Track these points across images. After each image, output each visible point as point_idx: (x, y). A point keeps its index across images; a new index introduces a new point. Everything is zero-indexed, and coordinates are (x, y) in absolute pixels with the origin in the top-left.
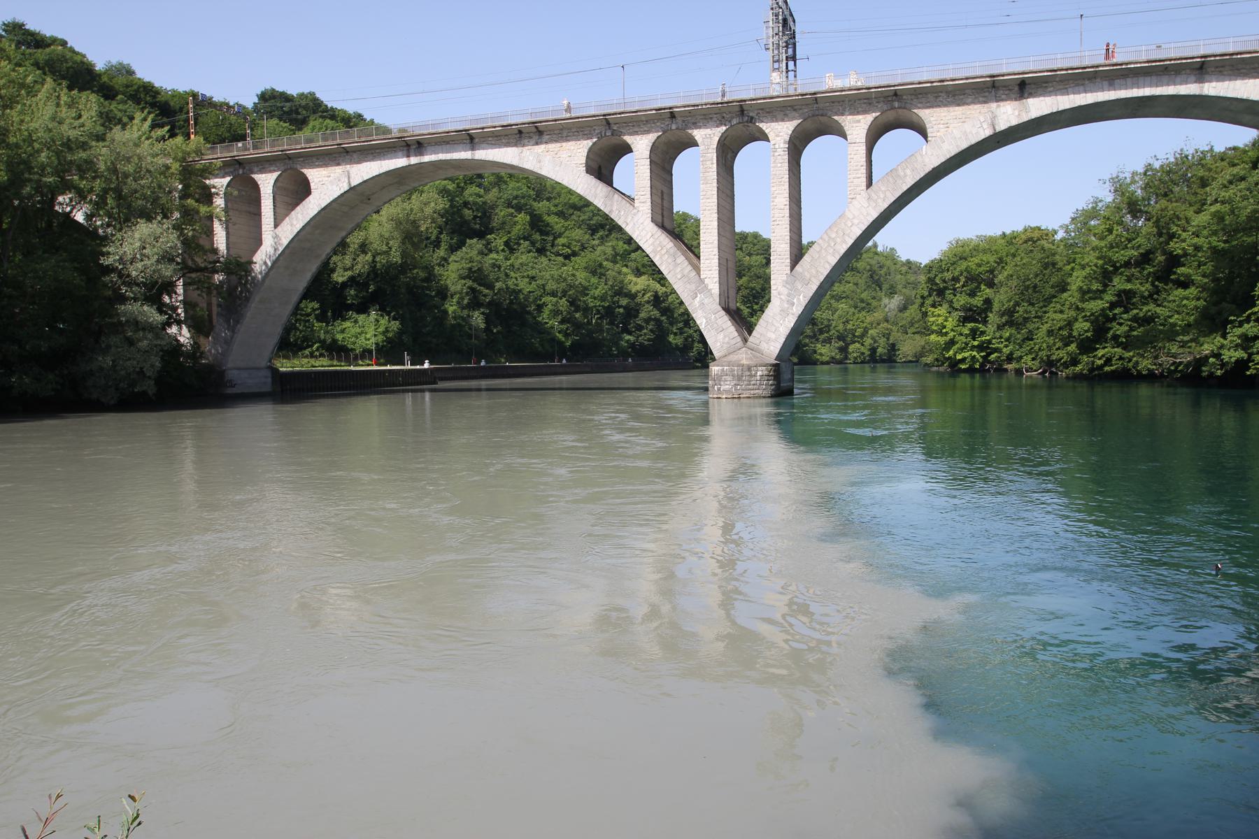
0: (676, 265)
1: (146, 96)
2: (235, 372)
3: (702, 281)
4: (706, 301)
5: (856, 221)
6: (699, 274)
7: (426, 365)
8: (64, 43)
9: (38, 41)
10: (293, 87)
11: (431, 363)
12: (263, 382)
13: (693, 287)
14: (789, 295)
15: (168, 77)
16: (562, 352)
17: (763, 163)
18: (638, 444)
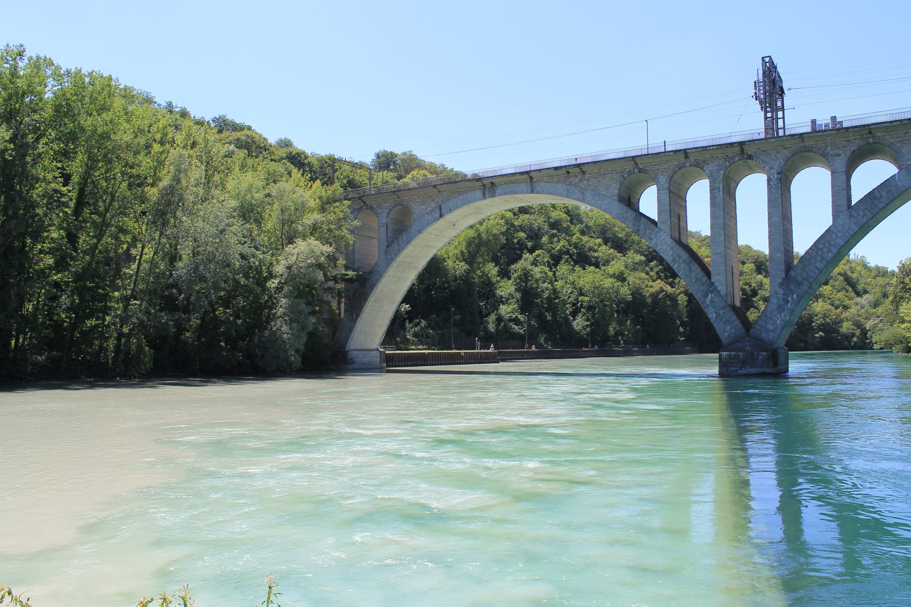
0: (691, 271)
1: (297, 160)
2: (356, 352)
3: (713, 284)
4: (716, 299)
5: (840, 235)
6: (710, 278)
7: (491, 350)
8: (249, 128)
9: (237, 128)
10: (398, 148)
11: (495, 348)
12: (375, 358)
13: (705, 288)
14: (784, 294)
15: (314, 145)
16: (520, 340)
17: (752, 192)
18: (339, 303)
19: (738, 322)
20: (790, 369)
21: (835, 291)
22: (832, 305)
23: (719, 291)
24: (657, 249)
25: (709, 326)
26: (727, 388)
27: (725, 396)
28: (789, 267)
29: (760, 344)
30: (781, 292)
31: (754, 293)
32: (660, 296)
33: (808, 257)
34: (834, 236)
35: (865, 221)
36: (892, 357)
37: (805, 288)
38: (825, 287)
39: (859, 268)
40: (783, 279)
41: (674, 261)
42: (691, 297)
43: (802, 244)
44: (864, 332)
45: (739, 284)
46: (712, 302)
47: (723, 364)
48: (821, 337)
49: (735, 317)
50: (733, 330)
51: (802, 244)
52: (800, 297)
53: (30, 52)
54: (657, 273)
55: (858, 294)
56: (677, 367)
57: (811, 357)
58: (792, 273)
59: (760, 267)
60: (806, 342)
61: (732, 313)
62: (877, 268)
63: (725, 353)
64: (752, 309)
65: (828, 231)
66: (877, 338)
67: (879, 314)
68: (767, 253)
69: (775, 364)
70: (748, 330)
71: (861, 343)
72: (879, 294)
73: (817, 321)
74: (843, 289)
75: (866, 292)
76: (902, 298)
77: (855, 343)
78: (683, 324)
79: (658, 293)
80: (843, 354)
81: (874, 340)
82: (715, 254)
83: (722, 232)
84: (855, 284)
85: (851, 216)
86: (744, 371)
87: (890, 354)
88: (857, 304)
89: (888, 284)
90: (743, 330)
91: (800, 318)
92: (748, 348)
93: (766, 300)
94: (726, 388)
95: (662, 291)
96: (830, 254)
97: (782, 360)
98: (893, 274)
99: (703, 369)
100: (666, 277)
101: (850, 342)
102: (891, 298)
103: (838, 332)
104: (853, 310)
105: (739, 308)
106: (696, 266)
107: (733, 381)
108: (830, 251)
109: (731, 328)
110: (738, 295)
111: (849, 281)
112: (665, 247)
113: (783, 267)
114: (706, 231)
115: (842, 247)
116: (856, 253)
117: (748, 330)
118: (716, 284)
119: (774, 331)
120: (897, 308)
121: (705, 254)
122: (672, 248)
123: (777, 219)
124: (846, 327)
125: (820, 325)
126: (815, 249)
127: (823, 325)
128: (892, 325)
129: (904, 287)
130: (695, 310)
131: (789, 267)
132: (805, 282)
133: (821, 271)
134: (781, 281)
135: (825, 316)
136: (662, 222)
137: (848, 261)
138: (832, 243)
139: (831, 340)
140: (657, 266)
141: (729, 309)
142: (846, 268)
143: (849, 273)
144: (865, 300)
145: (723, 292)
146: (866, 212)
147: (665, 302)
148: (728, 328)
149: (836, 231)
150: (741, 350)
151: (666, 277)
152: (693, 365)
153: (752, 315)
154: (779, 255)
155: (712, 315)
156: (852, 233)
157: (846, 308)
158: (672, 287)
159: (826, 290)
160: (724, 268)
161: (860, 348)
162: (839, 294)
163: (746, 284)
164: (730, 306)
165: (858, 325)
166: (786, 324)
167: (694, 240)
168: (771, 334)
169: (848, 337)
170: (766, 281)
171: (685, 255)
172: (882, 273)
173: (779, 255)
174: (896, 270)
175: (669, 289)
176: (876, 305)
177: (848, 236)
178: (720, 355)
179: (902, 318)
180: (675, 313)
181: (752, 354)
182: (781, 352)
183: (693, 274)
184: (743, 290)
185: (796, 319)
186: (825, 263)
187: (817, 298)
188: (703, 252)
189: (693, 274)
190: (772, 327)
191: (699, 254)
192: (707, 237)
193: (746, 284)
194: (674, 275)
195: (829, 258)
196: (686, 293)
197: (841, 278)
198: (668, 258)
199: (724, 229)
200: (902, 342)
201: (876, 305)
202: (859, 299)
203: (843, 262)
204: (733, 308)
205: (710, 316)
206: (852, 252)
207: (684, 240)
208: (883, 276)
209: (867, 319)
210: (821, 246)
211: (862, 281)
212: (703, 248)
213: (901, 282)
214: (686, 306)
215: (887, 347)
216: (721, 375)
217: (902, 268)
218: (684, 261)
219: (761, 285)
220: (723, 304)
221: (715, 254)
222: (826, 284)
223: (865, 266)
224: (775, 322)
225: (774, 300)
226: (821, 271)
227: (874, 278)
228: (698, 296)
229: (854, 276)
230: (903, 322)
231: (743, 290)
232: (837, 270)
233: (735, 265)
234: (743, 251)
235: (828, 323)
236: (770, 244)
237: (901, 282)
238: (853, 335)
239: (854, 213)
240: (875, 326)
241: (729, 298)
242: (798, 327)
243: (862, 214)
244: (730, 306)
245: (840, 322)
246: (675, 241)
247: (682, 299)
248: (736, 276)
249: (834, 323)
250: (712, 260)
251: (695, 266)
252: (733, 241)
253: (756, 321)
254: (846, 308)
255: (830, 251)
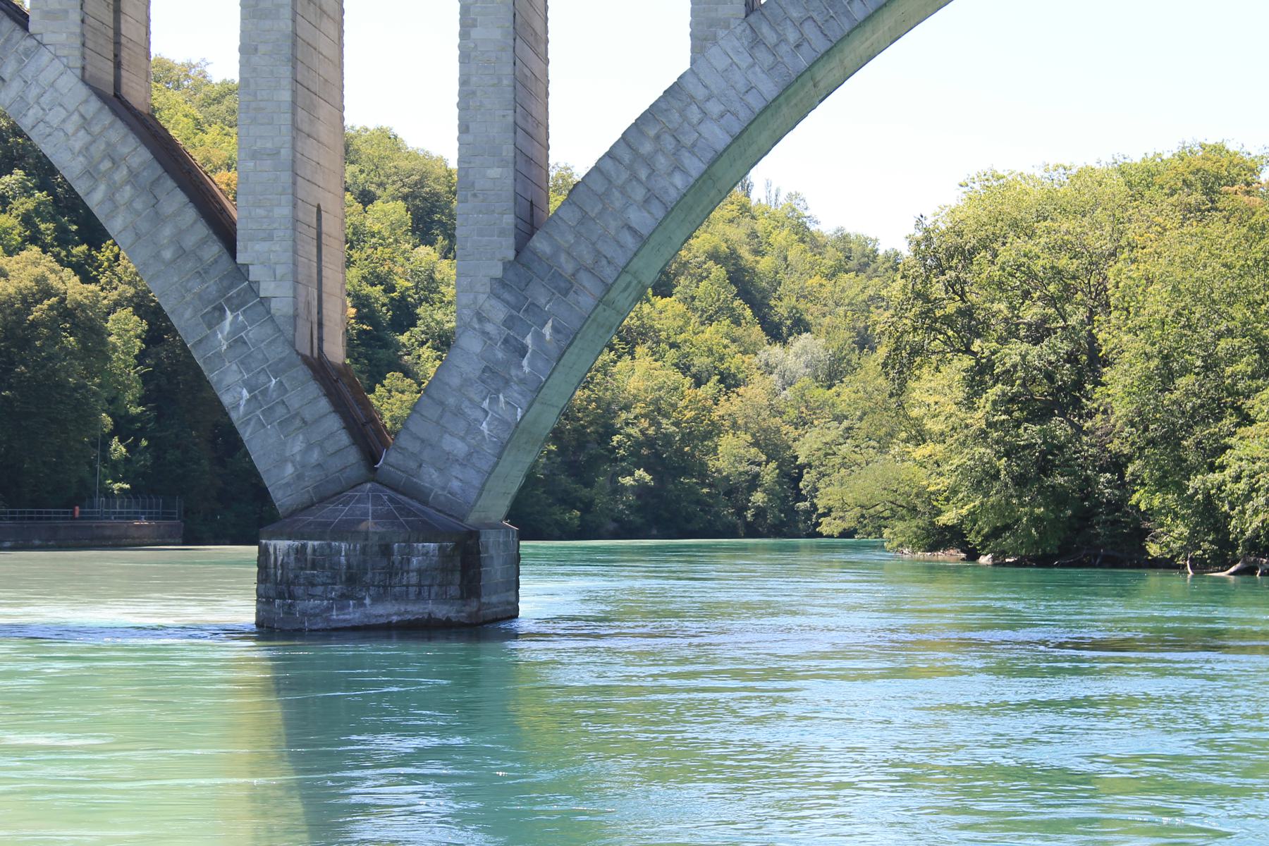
0: (158, 218)
3: (241, 272)
4: (252, 333)
5: (714, 108)
6: (232, 252)
13: (211, 286)
14: (509, 322)
19: (333, 423)
20: (522, 607)
21: (695, 319)
22: (684, 369)
23: (264, 301)
24: (26, 124)
25: (227, 440)
26: (284, 684)
27: (277, 712)
28: (530, 220)
29: (414, 510)
30: (499, 313)
31: (404, 315)
32: (37, 313)
33: (599, 186)
34: (694, 114)
35: (803, 63)
36: (878, 566)
37: (586, 301)
38: (660, 302)
39: (780, 237)
40: (507, 266)
41: (91, 173)
42: (158, 327)
43: (577, 141)
44: (792, 474)
45: (342, 282)
46: (237, 341)
47: (275, 589)
48: (641, 489)
49: (324, 404)
50: (315, 456)
51: (577, 141)
52: (568, 337)
53: (912, 230)
54: (26, 219)
55: (775, 333)
56: (95, 591)
57: (608, 560)
58: (539, 243)
59: (429, 217)
60: (587, 507)
61: (314, 389)
62: (843, 238)
63: (283, 544)
64: (393, 378)
65: (674, 92)
66: (836, 495)
67: (842, 408)
68: (453, 165)
69: (471, 586)
70: (371, 457)
71: (778, 514)
72: (844, 336)
73: (632, 428)
74: (724, 310)
75: (801, 325)
76: (916, 351)
77: (760, 512)
78: (123, 427)
79: (27, 301)
80: (755, 548)
81: (821, 504)
82: (255, 155)
83: (286, 71)
84: (765, 295)
85: (756, 41)
86: (353, 615)
87: (875, 556)
88: (768, 369)
89: (875, 299)
90: (353, 456)
91: (567, 414)
92: (369, 525)
93: (444, 342)
94: (280, 686)
95: (46, 291)
96: (678, 180)
97: (494, 570)
98: (894, 263)
99: (202, 601)
100: (63, 239)
101: (741, 511)
102: (882, 352)
103: (702, 472)
104: (756, 391)
105: (343, 371)
106: (180, 197)
107: (305, 651)
108: (678, 168)
109: (309, 447)
110: (340, 317)
111: (749, 290)
112: (55, 117)
113: (509, 219)
114: (224, 67)
115: (719, 156)
116: (776, 176)
117: (371, 457)
118: (255, 273)
119: (465, 462)
120: (900, 390)
121: (219, 155)
122: (85, 124)
123: (494, 33)
124: (729, 455)
125: (638, 444)
126: (626, 157)
127: (650, 442)
128: (883, 449)
129: (925, 314)
130: (173, 376)
131: (530, 220)
132: (585, 278)
133: (643, 241)
134: (498, 272)
135: (657, 410)
136: (49, 15)
137: (745, 209)
138: (688, 140)
139: (673, 499)
140: (27, 192)
141: (302, 372)
142: (737, 233)
143: (745, 253)
144: (797, 355)
145: (281, 307)
146: (809, 29)
147: (54, 338)
148: (296, 446)
149: (700, 93)
150: (344, 530)
151: (63, 239)
152: (169, 584)
153: (391, 401)
154: (495, 172)
155: (235, 395)
156: (757, 105)
157: (730, 382)
158: (86, 279)
159: (664, 312)
160: (286, 211)
161: (777, 531)
162: (709, 331)
163: (375, 279)
164: (306, 360)
165: (771, 446)
166: (514, 434)
167: (177, 96)
168: (456, 471)
169: (736, 490)
170: (446, 269)
171: (138, 155)
172: (856, 258)
173: (495, 172)
174: (906, 251)
175: (72, 286)
176: (833, 374)
177: (745, 115)
178: (264, 552)
179: (917, 423)
180: (94, 383)
181: (386, 550)
182: (492, 543)
183: (167, 231)
184: (361, 302)
185: (550, 420)
186: (660, 213)
187: (630, 341)
188: (211, 148)
189: (167, 231)
190: (460, 448)
191: (197, 156)
192: (227, 91)
193: (375, 279)
194: (94, 234)
195: (673, 195)
196: (144, 307)
197: (718, 272)
198: (69, 164)
199: (294, 60)
200: (913, 510)
201: (833, 374)
202: (777, 350)
203: (723, 211)
204: (319, 368)
205: (226, 399)
206: (757, 175)
207: (133, 92)
208: (862, 268)
209: (802, 423)
210: (647, 148)
211: (790, 283)
212: (213, 132)
213: (918, 295)
214: (140, 358)
215: (862, 533)
216: (266, 629)
217: (924, 243)
218: (133, 176)
219: (429, 285)
220: (280, 351)
221: (255, 155)
222: (664, 288)
223: (802, 232)
224: (472, 428)
225: (471, 344)
226: (643, 241)
227: (832, 276)
228: (184, 319)
229: (765, 264)
230: (920, 437)
231: (361, 302)
232: (703, 241)
233: (330, 204)
234: (366, 150)
235: (668, 438)
236: (464, 128)
237: (918, 295)
238: (754, 482)
239: (765, 30)
240: (829, 451)
241: (303, 331)
242: (562, 451)
243: (792, 36)
244: (306, 360)
245: (708, 435)
246: (100, 95)
247: (124, 329)
248: (334, 251)
249: (688, 437)
250: (244, 178)
251: (175, 201)
252: (324, 110)
253: (405, 422)
254: (730, 382)
255: (678, 168)
